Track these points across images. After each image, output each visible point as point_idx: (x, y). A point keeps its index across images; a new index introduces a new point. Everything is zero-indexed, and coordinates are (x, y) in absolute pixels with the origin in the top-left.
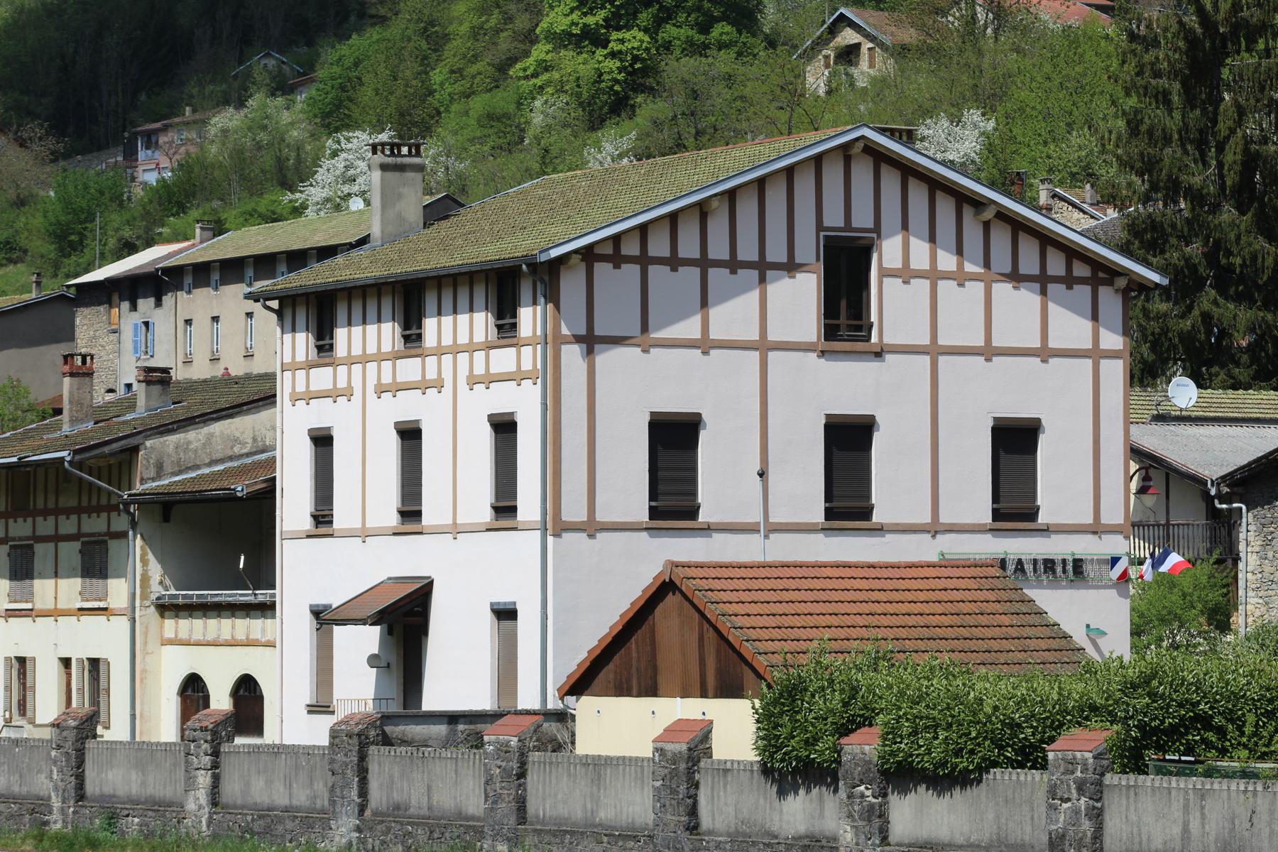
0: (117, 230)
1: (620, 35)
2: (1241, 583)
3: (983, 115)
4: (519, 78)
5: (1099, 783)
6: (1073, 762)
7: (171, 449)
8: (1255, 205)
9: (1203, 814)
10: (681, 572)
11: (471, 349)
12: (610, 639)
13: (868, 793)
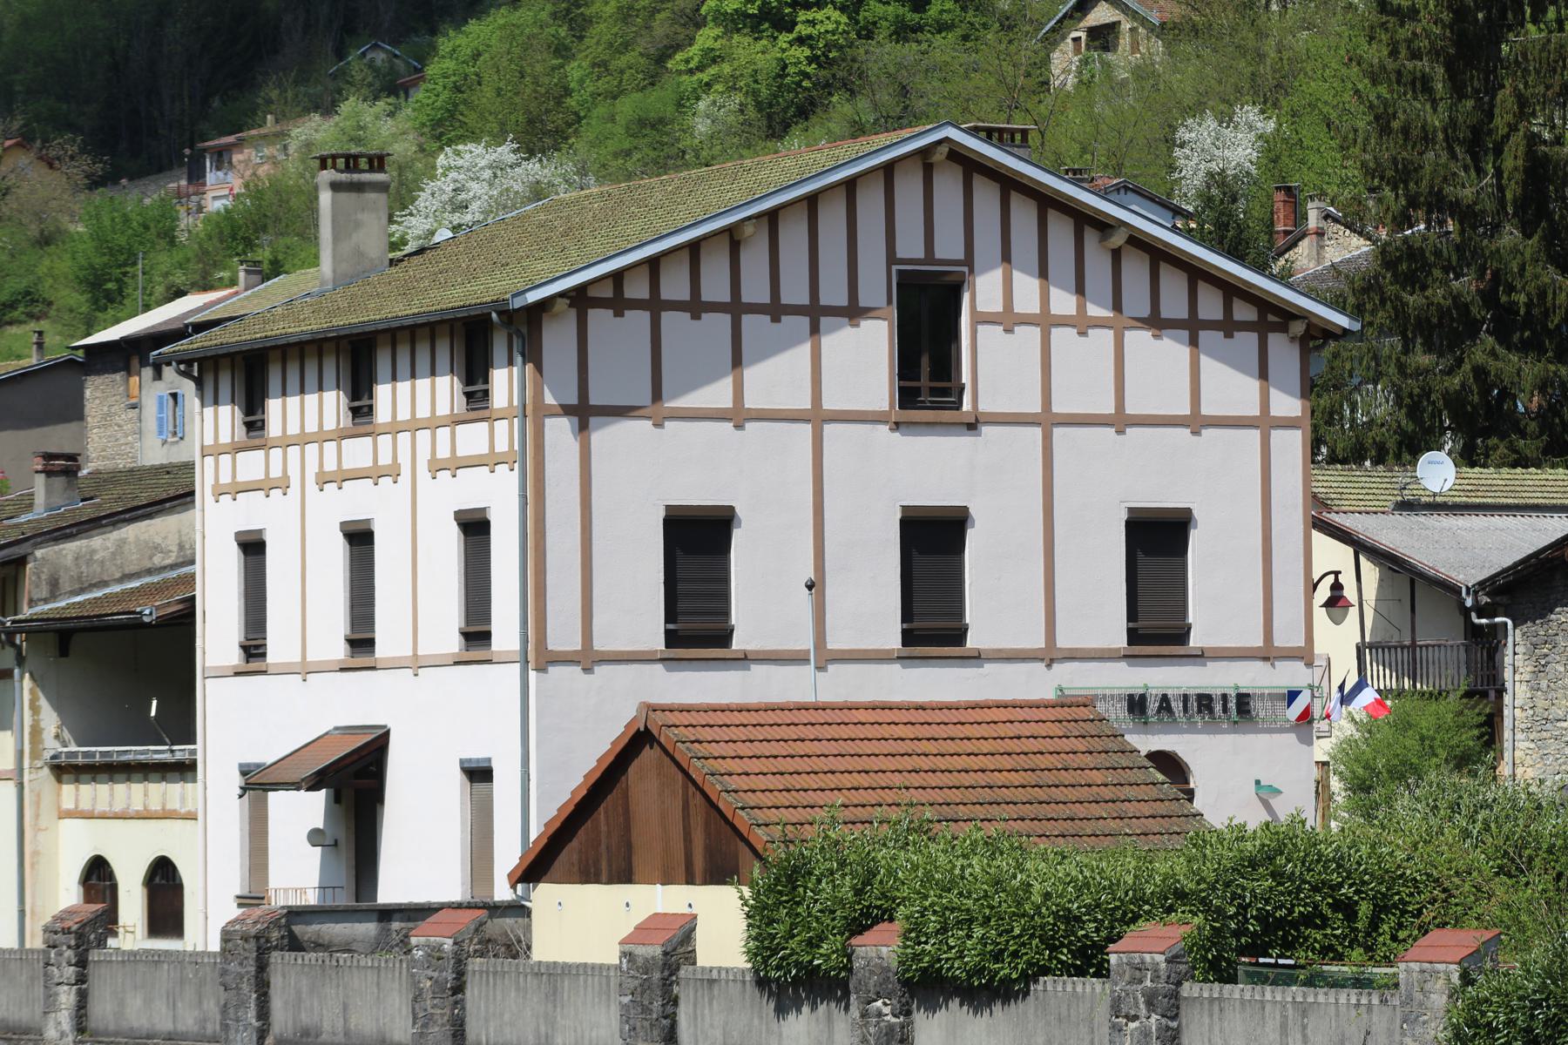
0: (166, 275)
1: (810, 15)
2: (1507, 723)
3: (1262, 112)
4: (680, 73)
5: (1175, 995)
6: (1140, 968)
7: (69, 561)
8: (1543, 224)
9: (1305, 1036)
10: (659, 718)
11: (433, 424)
12: (572, 808)
13: (887, 1010)
